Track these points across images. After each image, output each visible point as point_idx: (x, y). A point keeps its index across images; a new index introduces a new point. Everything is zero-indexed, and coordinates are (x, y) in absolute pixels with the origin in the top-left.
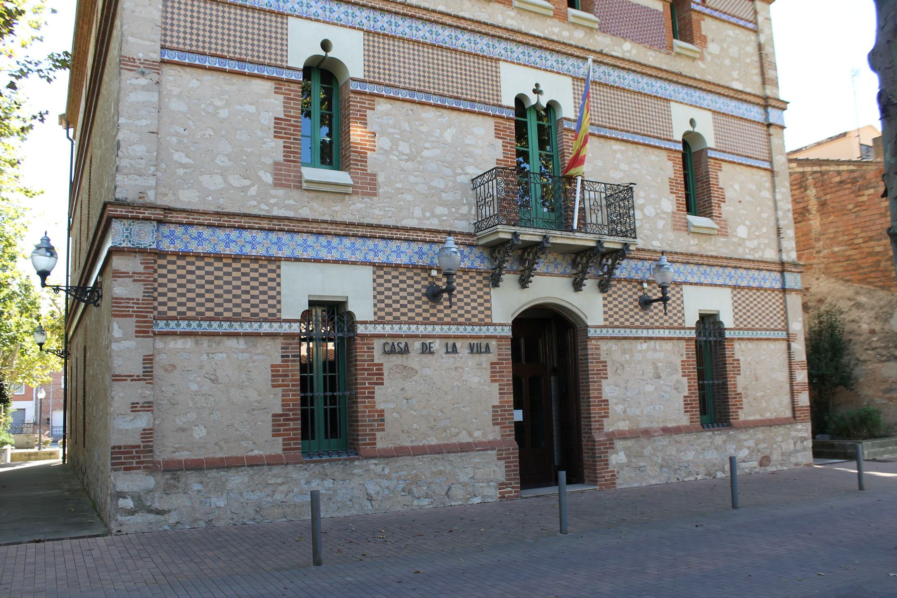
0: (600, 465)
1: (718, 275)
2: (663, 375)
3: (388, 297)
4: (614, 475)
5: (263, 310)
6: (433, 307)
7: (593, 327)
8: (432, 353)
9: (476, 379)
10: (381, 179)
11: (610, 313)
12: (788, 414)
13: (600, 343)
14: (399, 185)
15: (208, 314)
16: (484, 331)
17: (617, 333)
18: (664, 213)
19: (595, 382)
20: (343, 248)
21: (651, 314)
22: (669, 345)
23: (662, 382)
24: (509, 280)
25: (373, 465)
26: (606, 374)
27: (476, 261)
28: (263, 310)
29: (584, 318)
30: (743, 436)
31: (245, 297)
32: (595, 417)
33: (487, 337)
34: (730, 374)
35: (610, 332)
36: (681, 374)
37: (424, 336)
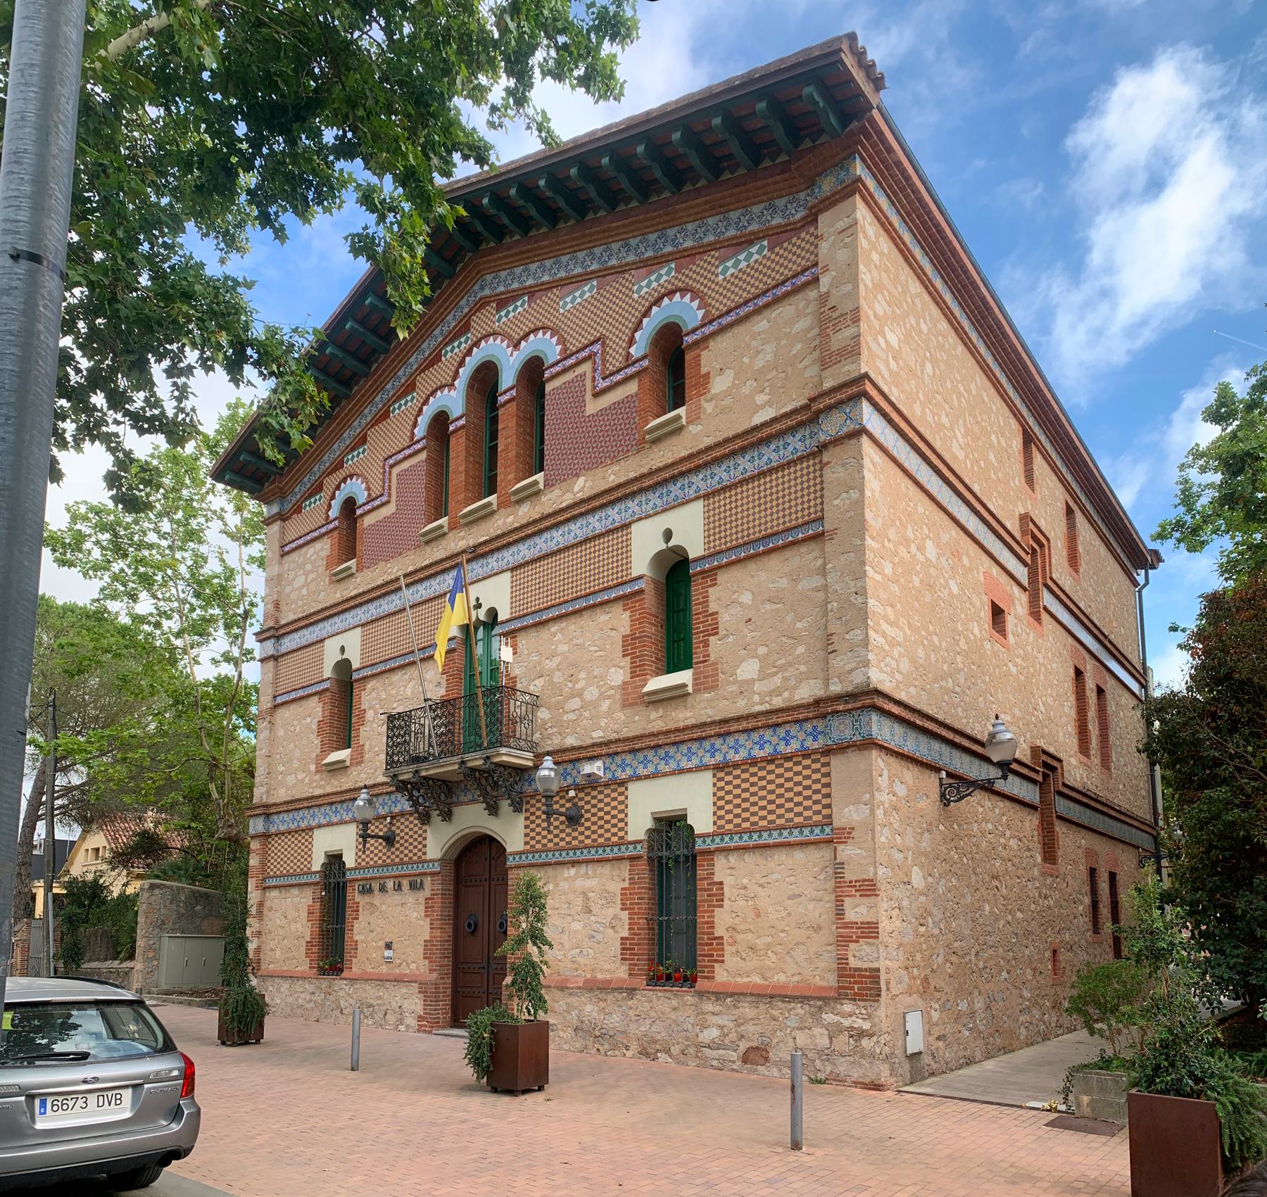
2: (595, 909)
9: (415, 915)
11: (533, 834)
12: (831, 980)
17: (537, 859)
18: (612, 688)
22: (606, 870)
23: (592, 918)
28: (779, 816)
30: (709, 1006)
33: (420, 874)
34: (703, 907)
35: (530, 859)
36: (619, 906)
37: (380, 878)
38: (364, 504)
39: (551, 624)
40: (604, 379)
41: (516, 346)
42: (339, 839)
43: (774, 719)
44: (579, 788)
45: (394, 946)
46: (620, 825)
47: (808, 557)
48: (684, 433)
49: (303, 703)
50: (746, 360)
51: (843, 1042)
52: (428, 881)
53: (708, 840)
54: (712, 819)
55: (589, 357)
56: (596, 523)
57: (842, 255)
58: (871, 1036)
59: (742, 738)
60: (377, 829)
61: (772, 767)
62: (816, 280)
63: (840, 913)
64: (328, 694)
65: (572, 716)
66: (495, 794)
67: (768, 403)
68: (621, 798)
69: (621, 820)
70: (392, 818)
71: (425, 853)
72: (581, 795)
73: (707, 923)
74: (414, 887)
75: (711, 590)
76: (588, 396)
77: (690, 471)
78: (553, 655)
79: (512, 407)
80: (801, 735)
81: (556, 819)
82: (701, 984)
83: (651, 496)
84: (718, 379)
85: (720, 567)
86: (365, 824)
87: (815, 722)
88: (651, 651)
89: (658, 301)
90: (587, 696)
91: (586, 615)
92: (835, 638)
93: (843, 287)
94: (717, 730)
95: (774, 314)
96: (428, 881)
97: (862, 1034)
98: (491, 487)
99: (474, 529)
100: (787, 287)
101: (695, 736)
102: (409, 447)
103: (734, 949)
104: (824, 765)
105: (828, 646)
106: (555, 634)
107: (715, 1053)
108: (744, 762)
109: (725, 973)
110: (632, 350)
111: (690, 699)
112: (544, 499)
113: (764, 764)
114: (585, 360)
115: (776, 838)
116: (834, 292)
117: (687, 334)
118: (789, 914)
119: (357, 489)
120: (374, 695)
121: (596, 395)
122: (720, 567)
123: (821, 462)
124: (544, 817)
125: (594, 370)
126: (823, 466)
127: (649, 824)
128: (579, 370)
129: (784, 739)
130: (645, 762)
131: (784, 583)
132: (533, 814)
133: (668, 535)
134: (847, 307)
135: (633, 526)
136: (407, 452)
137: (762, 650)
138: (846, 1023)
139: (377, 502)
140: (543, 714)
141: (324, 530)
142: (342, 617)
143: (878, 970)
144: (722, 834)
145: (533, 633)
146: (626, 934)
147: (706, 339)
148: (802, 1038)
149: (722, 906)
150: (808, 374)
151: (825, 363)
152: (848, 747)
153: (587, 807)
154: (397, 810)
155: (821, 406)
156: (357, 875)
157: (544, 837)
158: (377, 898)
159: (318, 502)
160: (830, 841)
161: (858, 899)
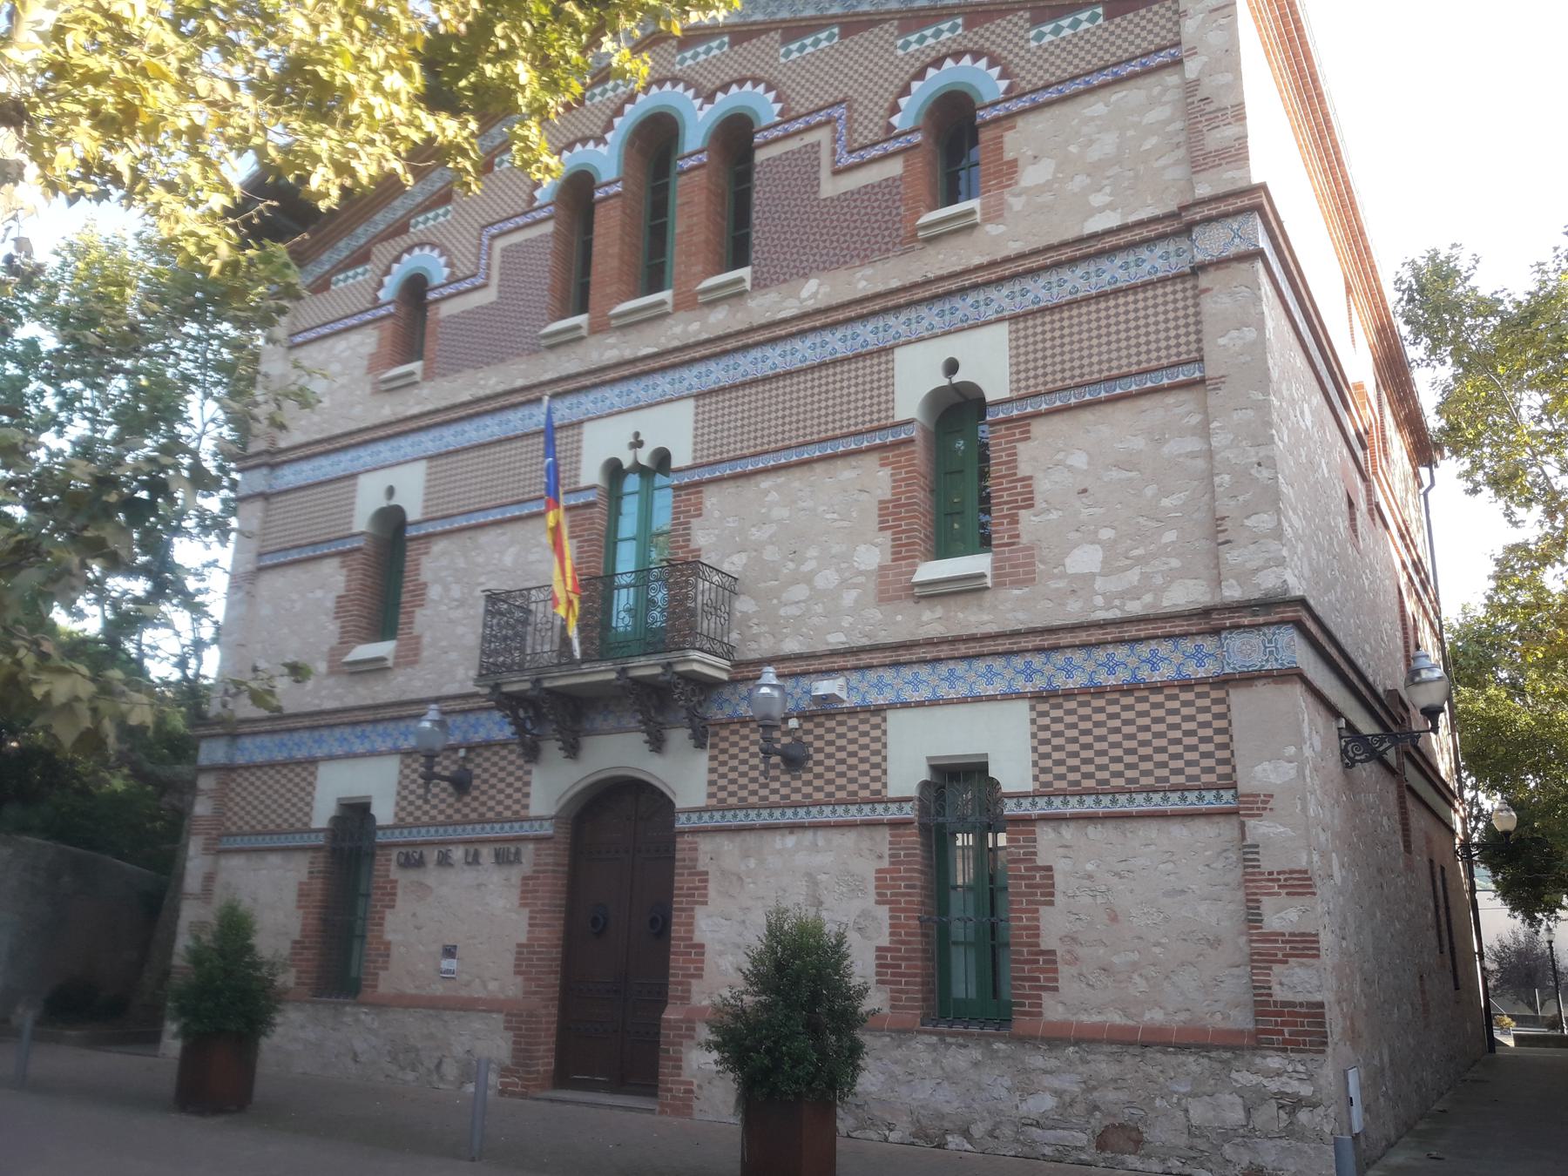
0: (665, 1069)
1: (916, 683)
3: (1143, 743)
4: (691, 1091)
5: (1145, 773)
6: (458, 800)
7: (683, 811)
8: (451, 865)
10: (426, 640)
12: (1242, 1020)
13: (699, 839)
14: (444, 643)
15: (1144, 781)
16: (517, 830)
17: (730, 819)
18: (861, 573)
19: (683, 910)
20: (974, 678)
21: (807, 777)
22: (849, 839)
24: (552, 749)
25: (366, 1016)
26: (706, 896)
27: (496, 727)
28: (1145, 773)
29: (668, 793)
30: (1037, 1060)
31: (1147, 751)
32: (676, 975)
35: (718, 819)
36: (872, 897)
37: (442, 843)
38: (442, 286)
39: (759, 478)
40: (850, 152)
41: (710, 98)
42: (376, 781)
43: (1132, 632)
44: (804, 716)
45: (459, 953)
46: (874, 773)
47: (1177, 410)
48: (977, 233)
49: (311, 567)
50: (1073, 149)
51: (1267, 1115)
52: (528, 849)
53: (1026, 803)
54: (1030, 772)
55: (828, 122)
56: (836, 343)
57: (1215, 38)
58: (1315, 1106)
59: (1078, 657)
60: (446, 766)
61: (1130, 700)
62: (1178, 63)
63: (1253, 917)
64: (358, 556)
65: (793, 611)
66: (660, 719)
67: (1111, 207)
68: (876, 733)
69: (876, 766)
70: (470, 749)
71: (526, 807)
72: (808, 726)
73: (1027, 928)
74: (502, 859)
75: (1021, 446)
76: (825, 173)
77: (988, 284)
78: (765, 521)
79: (700, 177)
80: (1009, 674)
81: (437, 785)
82: (1021, 1024)
83: (924, 311)
84: (1030, 169)
85: (1037, 415)
86: (430, 757)
87: (1199, 640)
88: (920, 527)
89: (937, 63)
90: (820, 582)
91: (819, 468)
92: (1227, 524)
93: (1219, 76)
94: (1037, 641)
95: (1114, 98)
96: (528, 849)
97: (1298, 1103)
98: (655, 281)
99: (633, 335)
100: (1079, 85)
101: (1000, 649)
102: (525, 213)
103: (1074, 970)
104: (1216, 702)
105: (1218, 531)
106: (767, 492)
107: (1050, 1135)
108: (1084, 691)
109: (1060, 1008)
110: (381, 294)
111: (988, 595)
112: (751, 303)
113: (1116, 696)
114: (820, 125)
115: (1140, 803)
116: (1206, 80)
117: (984, 108)
118: (1167, 919)
119: (435, 266)
120: (444, 562)
121: (836, 172)
122: (1037, 415)
123: (1195, 287)
124: (421, 781)
125: (835, 141)
126: (1199, 293)
127: (924, 774)
128: (810, 138)
129: (1148, 661)
130: (990, 675)
131: (1139, 443)
132: (724, 751)
133: (952, 367)
134: (1228, 101)
135: (897, 351)
136: (520, 221)
137: (1106, 534)
138: (1273, 1086)
139: (466, 285)
140: (744, 605)
141: (368, 317)
142: (393, 443)
143: (1321, 1005)
144: (1049, 795)
145: (729, 489)
146: (885, 941)
147: (1011, 116)
148: (1199, 1112)
149: (1051, 903)
150: (1170, 175)
151: (1199, 162)
152: (1259, 677)
153: (818, 744)
154: (479, 737)
155: (1198, 217)
156: (398, 837)
157: (419, 808)
158: (431, 875)
159: (361, 276)
160: (1233, 813)
161: (1283, 899)
